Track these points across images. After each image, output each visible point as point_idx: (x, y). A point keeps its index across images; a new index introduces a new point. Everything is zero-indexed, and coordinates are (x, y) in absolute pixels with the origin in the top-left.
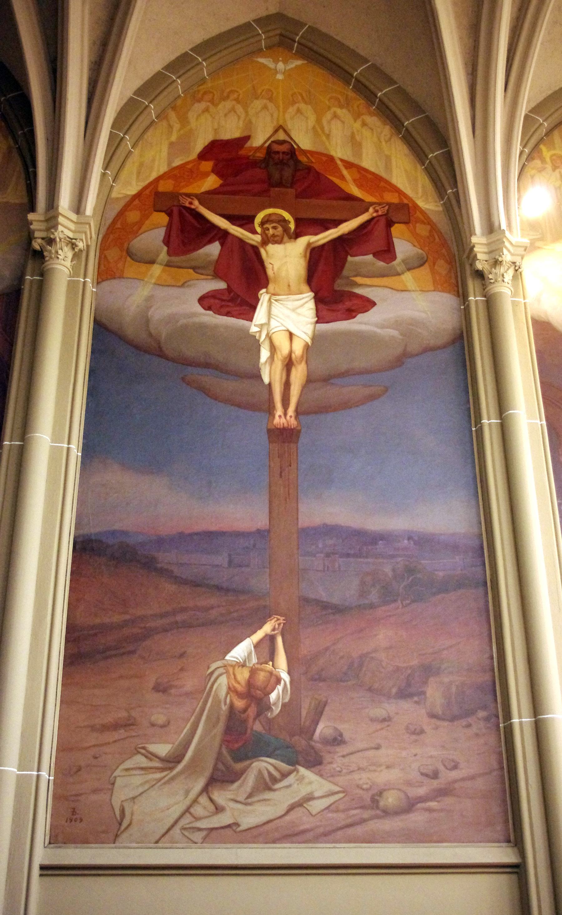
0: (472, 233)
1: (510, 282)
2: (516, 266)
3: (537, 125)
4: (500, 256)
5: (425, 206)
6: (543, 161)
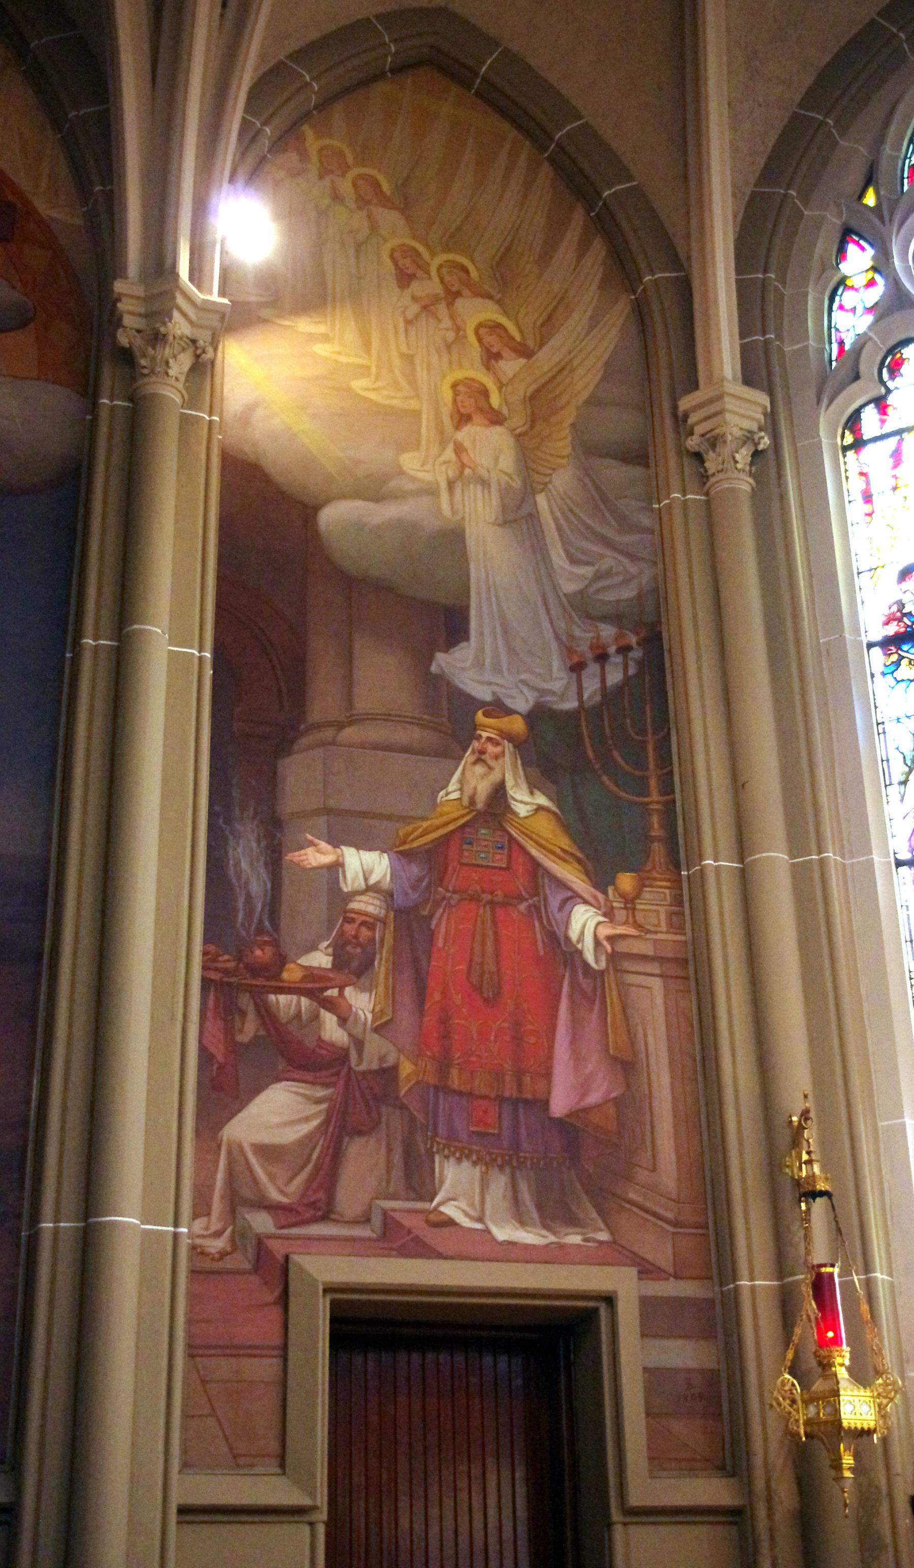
0: (119, 271)
1: (182, 378)
2: (197, 348)
3: (298, 84)
4: (164, 324)
5: (49, 212)
6: (304, 155)
